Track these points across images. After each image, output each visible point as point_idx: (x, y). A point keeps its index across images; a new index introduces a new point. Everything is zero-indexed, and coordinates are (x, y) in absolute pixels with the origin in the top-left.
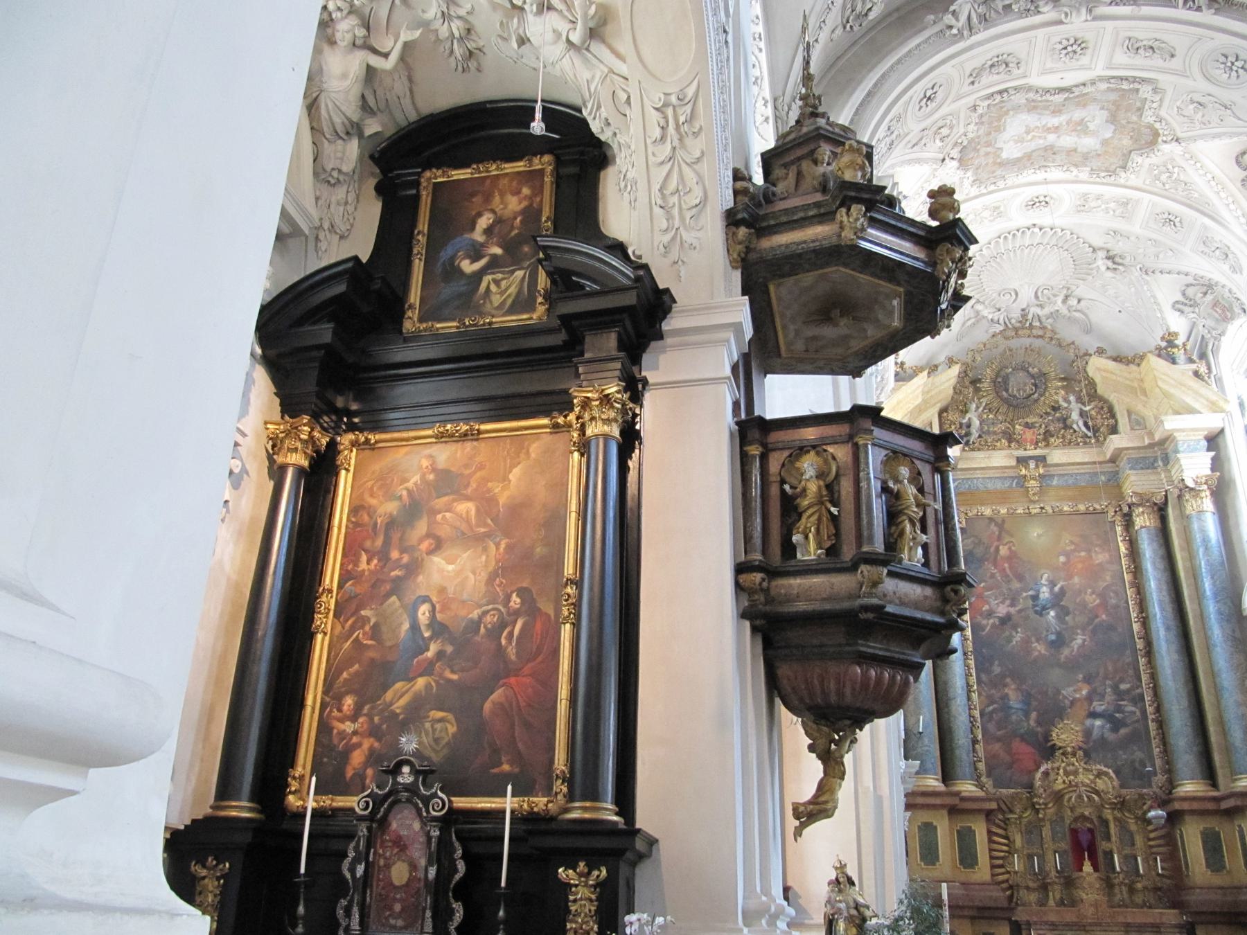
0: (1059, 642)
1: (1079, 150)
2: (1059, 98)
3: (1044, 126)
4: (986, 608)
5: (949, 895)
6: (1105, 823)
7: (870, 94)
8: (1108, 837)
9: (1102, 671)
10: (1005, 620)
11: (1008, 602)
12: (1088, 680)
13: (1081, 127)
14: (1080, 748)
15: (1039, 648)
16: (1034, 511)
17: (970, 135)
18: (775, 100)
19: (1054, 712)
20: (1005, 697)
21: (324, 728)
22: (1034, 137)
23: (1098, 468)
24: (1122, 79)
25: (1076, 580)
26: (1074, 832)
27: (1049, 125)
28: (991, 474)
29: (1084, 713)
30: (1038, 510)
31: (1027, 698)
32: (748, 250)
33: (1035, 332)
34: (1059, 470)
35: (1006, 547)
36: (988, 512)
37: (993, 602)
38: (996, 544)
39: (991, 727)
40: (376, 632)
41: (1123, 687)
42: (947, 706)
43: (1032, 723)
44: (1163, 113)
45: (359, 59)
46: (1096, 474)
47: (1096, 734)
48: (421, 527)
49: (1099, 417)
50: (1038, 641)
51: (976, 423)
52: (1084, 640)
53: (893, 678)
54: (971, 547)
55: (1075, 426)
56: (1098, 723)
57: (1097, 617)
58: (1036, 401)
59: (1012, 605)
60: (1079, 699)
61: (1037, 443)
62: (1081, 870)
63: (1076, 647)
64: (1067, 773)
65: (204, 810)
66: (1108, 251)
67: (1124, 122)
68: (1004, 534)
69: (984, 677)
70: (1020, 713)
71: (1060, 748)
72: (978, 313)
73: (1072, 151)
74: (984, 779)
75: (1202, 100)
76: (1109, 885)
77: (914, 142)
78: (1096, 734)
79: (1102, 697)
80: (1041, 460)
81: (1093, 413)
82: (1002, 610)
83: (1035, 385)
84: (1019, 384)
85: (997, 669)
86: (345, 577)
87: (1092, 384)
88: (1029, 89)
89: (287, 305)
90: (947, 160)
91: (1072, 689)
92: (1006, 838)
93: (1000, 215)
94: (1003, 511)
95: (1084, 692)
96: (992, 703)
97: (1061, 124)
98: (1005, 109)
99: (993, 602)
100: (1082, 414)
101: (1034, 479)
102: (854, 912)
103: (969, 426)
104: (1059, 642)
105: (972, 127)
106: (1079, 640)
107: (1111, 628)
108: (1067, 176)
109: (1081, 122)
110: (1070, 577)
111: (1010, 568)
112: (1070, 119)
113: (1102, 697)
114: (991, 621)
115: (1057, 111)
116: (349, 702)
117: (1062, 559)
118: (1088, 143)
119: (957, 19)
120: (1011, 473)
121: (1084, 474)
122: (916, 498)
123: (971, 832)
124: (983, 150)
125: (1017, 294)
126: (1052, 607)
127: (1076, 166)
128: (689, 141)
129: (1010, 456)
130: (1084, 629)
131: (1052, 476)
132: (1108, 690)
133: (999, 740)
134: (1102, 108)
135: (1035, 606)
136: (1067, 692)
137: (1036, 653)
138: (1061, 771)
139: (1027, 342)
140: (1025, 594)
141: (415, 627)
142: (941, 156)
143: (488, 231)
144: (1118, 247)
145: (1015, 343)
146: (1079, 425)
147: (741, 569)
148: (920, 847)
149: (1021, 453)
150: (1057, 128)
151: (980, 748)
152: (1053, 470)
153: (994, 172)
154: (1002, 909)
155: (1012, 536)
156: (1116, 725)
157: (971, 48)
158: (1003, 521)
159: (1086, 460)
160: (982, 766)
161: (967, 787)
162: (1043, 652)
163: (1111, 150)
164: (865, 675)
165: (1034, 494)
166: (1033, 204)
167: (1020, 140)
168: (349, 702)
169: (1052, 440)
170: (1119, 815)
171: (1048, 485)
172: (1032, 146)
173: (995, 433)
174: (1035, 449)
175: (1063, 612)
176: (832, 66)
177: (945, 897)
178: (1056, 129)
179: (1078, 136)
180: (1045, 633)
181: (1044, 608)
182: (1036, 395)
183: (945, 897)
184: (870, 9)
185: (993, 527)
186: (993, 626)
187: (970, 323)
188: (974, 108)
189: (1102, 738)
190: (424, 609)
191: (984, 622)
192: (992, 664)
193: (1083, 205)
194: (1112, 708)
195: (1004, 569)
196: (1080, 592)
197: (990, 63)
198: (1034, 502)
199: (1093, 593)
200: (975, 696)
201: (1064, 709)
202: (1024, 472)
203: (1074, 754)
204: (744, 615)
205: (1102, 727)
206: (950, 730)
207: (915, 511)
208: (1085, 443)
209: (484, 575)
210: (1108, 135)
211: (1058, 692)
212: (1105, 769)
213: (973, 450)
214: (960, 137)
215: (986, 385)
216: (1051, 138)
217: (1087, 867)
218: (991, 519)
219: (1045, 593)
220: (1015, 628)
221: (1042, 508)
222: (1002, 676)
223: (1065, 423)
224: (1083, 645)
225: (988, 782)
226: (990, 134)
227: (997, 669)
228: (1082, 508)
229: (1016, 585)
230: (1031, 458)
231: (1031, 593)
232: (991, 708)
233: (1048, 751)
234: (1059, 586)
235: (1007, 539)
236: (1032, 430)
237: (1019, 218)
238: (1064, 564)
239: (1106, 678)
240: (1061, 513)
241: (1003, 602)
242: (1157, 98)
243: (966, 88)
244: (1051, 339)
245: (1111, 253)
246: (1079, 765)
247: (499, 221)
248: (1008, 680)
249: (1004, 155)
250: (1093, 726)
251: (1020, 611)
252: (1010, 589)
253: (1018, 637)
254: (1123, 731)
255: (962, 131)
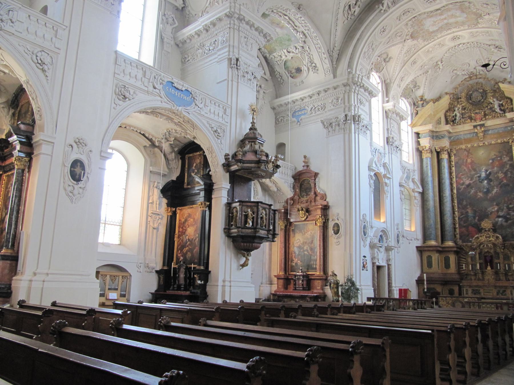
0: (488, 191)
2: (439, 11)
4: (462, 182)
5: (426, 277)
6: (498, 254)
7: (358, 40)
8: (499, 258)
9: (503, 201)
10: (469, 186)
11: (470, 179)
12: (497, 205)
13: (452, 16)
14: (491, 229)
15: (480, 194)
16: (480, 145)
17: (411, 31)
18: (328, 51)
19: (484, 216)
20: (467, 212)
21: (177, 255)
22: (438, 23)
23: (506, 125)
24: (456, 2)
25: (496, 168)
26: (485, 257)
28: (466, 132)
29: (496, 216)
30: (482, 144)
31: (475, 212)
32: (228, 170)
33: (478, 77)
34: (491, 128)
35: (470, 159)
36: (463, 147)
37: (464, 180)
38: (466, 158)
39: (462, 223)
40: (182, 241)
41: (510, 206)
42: (443, 217)
43: (476, 221)
44: (478, 7)
45: (167, 144)
46: (506, 127)
47: (499, 223)
48: (187, 223)
49: (507, 105)
50: (480, 192)
51: (458, 115)
52: (497, 190)
53: (249, 245)
54: (457, 161)
55: (496, 110)
56: (500, 219)
57: (502, 181)
58: (483, 102)
59: (471, 180)
60: (494, 212)
61: (482, 119)
62: (486, 269)
63: (494, 193)
64: (486, 237)
65: (161, 269)
66: (495, 45)
68: (469, 154)
69: (460, 206)
70: (472, 218)
71: (484, 229)
72: (456, 74)
73: (456, 23)
74: (458, 240)
75: (487, 3)
76: (497, 273)
77: (388, 41)
78: (499, 223)
79: (502, 210)
80: (482, 125)
82: (467, 182)
83: (482, 96)
84: (477, 96)
85: (465, 203)
86: (179, 232)
87: (503, 93)
88: (425, 13)
89: (208, 139)
91: (491, 208)
92: (465, 259)
93: (443, 45)
94: (469, 146)
95: (496, 209)
96: (462, 214)
99: (464, 180)
100: (500, 106)
101: (481, 132)
102: (336, 282)
103: (456, 115)
104: (488, 191)
105: (409, 29)
106: (495, 190)
107: (508, 185)
108: (459, 29)
109: (452, 15)
110: (493, 168)
111: (471, 167)
113: (502, 210)
114: (463, 186)
115: (441, 15)
116: (179, 251)
117: (491, 161)
118: (460, 19)
119: (383, 7)
120: (472, 131)
121: (501, 128)
122: (251, 214)
123: (449, 258)
124: (421, 32)
125: (469, 64)
126: (486, 180)
127: (462, 26)
128: (213, 154)
129: (471, 125)
130: (497, 187)
131: (489, 130)
132: (505, 208)
133: (464, 227)
135: (479, 180)
136: (490, 209)
137: (479, 197)
138: (484, 237)
139: (476, 81)
140: (476, 176)
141: (186, 240)
142: (404, 40)
143: (195, 167)
144: (497, 44)
145: (471, 82)
146: (498, 110)
147: (225, 229)
148: (427, 263)
149: (475, 124)
151: (458, 231)
152: (489, 128)
154: (456, 281)
155: (472, 154)
156: (507, 220)
157: (392, 12)
158: (469, 150)
159: (501, 123)
160: (458, 236)
161: (450, 244)
162: (481, 196)
164: (244, 245)
165: (481, 138)
166: (454, 39)
167: (433, 25)
168: (179, 251)
169: (487, 117)
170: (502, 251)
171: (487, 134)
172: (440, 25)
173: (465, 117)
174: (480, 121)
175: (490, 181)
176: (348, 31)
177: (425, 278)
178: (445, 19)
180: (482, 189)
181: (483, 180)
182: (482, 100)
183: (425, 278)
184: (355, 12)
185: (466, 153)
186: (464, 188)
187: (454, 77)
188: (407, 24)
189: (502, 225)
190: (187, 237)
191: (461, 187)
192: (463, 201)
193: (472, 35)
194: (506, 214)
195: (469, 167)
196: (497, 173)
197: (403, 13)
198: (482, 141)
199: (501, 173)
200: (456, 213)
201: (488, 215)
202: (476, 131)
203: (489, 231)
204: (226, 236)
205: (502, 221)
206: (444, 225)
207: (250, 216)
208: (501, 116)
209: (194, 231)
210: (466, 16)
211: (486, 209)
212: (499, 235)
213: (458, 125)
215: (462, 99)
216: (445, 21)
217: (489, 268)
218: (465, 150)
219: (483, 175)
220: (472, 188)
221: (484, 143)
222: (467, 205)
223: (492, 109)
224: (496, 193)
225: (460, 242)
226: (420, 27)
227: (465, 203)
228: (499, 141)
229: (473, 173)
230: (479, 125)
231: (478, 175)
232: (462, 216)
233: (480, 230)
234: (489, 172)
235: (471, 156)
236: (479, 115)
237: (452, 44)
238: (491, 163)
239: (504, 203)
240: (491, 144)
241: (468, 179)
242: (471, 5)
243: (398, 22)
244: (485, 78)
245: (496, 46)
246: (491, 234)
247: (196, 165)
248: (468, 206)
249: (431, 30)
250: (498, 221)
251: (474, 182)
252: (471, 175)
253: (473, 191)
254: (510, 222)
255: (407, 31)
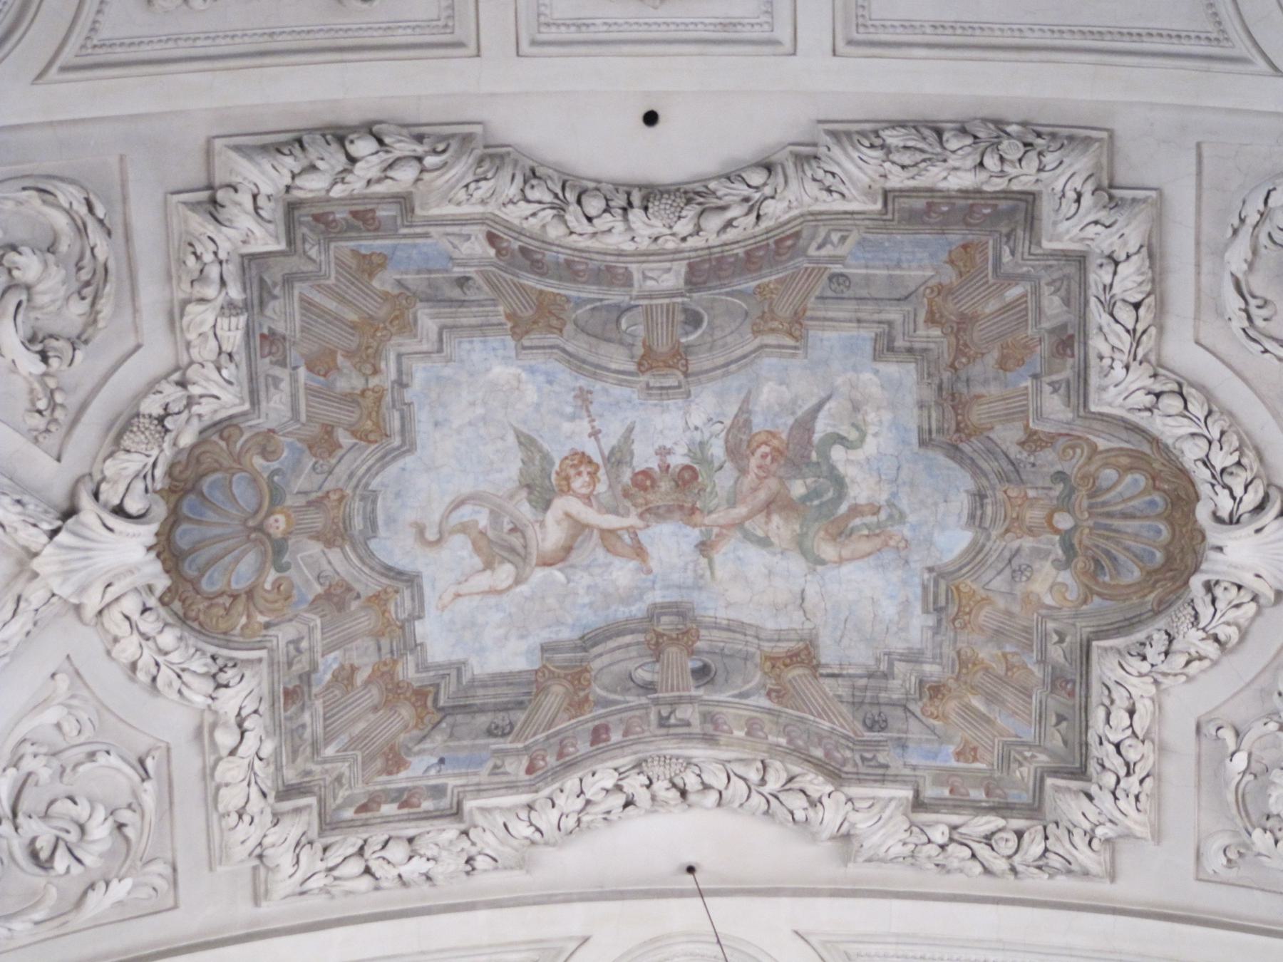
1: (828, 655)
3: (617, 458)
27: (644, 458)
67: (1008, 436)
81: (1110, 474)
90: (89, 512)
97: (699, 450)
98: (384, 282)
112: (742, 422)
134: (885, 348)
150: (686, 479)
153: (395, 760)
163: (986, 653)
179: (801, 546)
214: (152, 387)
242: (1132, 233)
